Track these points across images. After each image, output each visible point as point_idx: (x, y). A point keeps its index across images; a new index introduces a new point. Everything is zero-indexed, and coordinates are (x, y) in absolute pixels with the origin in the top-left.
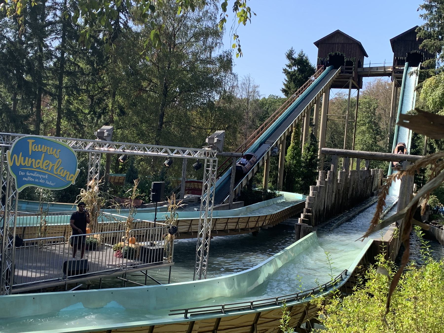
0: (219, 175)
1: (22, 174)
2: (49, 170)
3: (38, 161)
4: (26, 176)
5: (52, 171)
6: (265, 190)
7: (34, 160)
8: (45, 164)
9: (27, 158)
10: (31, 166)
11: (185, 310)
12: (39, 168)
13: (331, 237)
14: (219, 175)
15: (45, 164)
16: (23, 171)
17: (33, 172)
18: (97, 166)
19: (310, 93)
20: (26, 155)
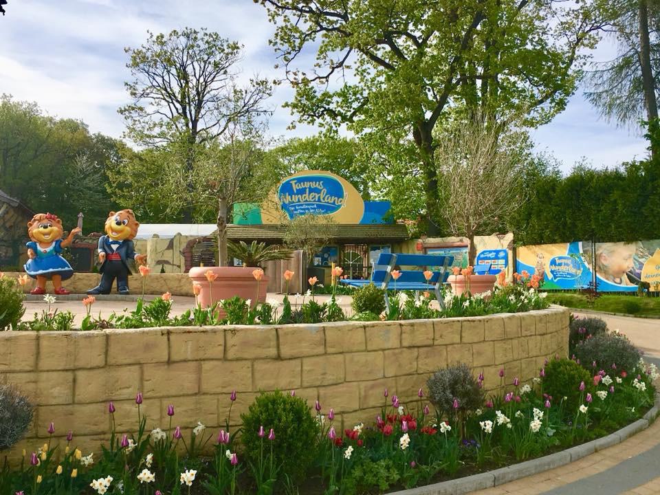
0: (277, 468)
1: (293, 208)
2: (317, 200)
3: (304, 195)
4: (296, 210)
5: (319, 200)
6: (338, 199)
7: (336, 198)
8: (311, 197)
9: (293, 196)
10: (299, 201)
11: (494, 251)
12: (307, 201)
13: (630, 245)
14: (277, 468)
15: (311, 197)
16: (292, 206)
17: (302, 205)
18: (502, 208)
19: (434, 248)
20: (291, 193)
